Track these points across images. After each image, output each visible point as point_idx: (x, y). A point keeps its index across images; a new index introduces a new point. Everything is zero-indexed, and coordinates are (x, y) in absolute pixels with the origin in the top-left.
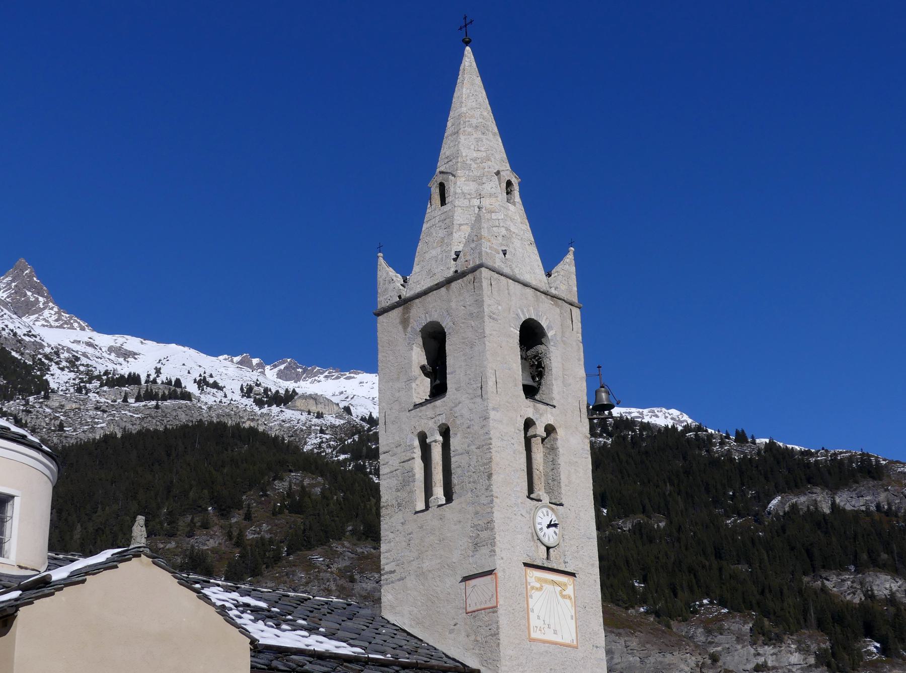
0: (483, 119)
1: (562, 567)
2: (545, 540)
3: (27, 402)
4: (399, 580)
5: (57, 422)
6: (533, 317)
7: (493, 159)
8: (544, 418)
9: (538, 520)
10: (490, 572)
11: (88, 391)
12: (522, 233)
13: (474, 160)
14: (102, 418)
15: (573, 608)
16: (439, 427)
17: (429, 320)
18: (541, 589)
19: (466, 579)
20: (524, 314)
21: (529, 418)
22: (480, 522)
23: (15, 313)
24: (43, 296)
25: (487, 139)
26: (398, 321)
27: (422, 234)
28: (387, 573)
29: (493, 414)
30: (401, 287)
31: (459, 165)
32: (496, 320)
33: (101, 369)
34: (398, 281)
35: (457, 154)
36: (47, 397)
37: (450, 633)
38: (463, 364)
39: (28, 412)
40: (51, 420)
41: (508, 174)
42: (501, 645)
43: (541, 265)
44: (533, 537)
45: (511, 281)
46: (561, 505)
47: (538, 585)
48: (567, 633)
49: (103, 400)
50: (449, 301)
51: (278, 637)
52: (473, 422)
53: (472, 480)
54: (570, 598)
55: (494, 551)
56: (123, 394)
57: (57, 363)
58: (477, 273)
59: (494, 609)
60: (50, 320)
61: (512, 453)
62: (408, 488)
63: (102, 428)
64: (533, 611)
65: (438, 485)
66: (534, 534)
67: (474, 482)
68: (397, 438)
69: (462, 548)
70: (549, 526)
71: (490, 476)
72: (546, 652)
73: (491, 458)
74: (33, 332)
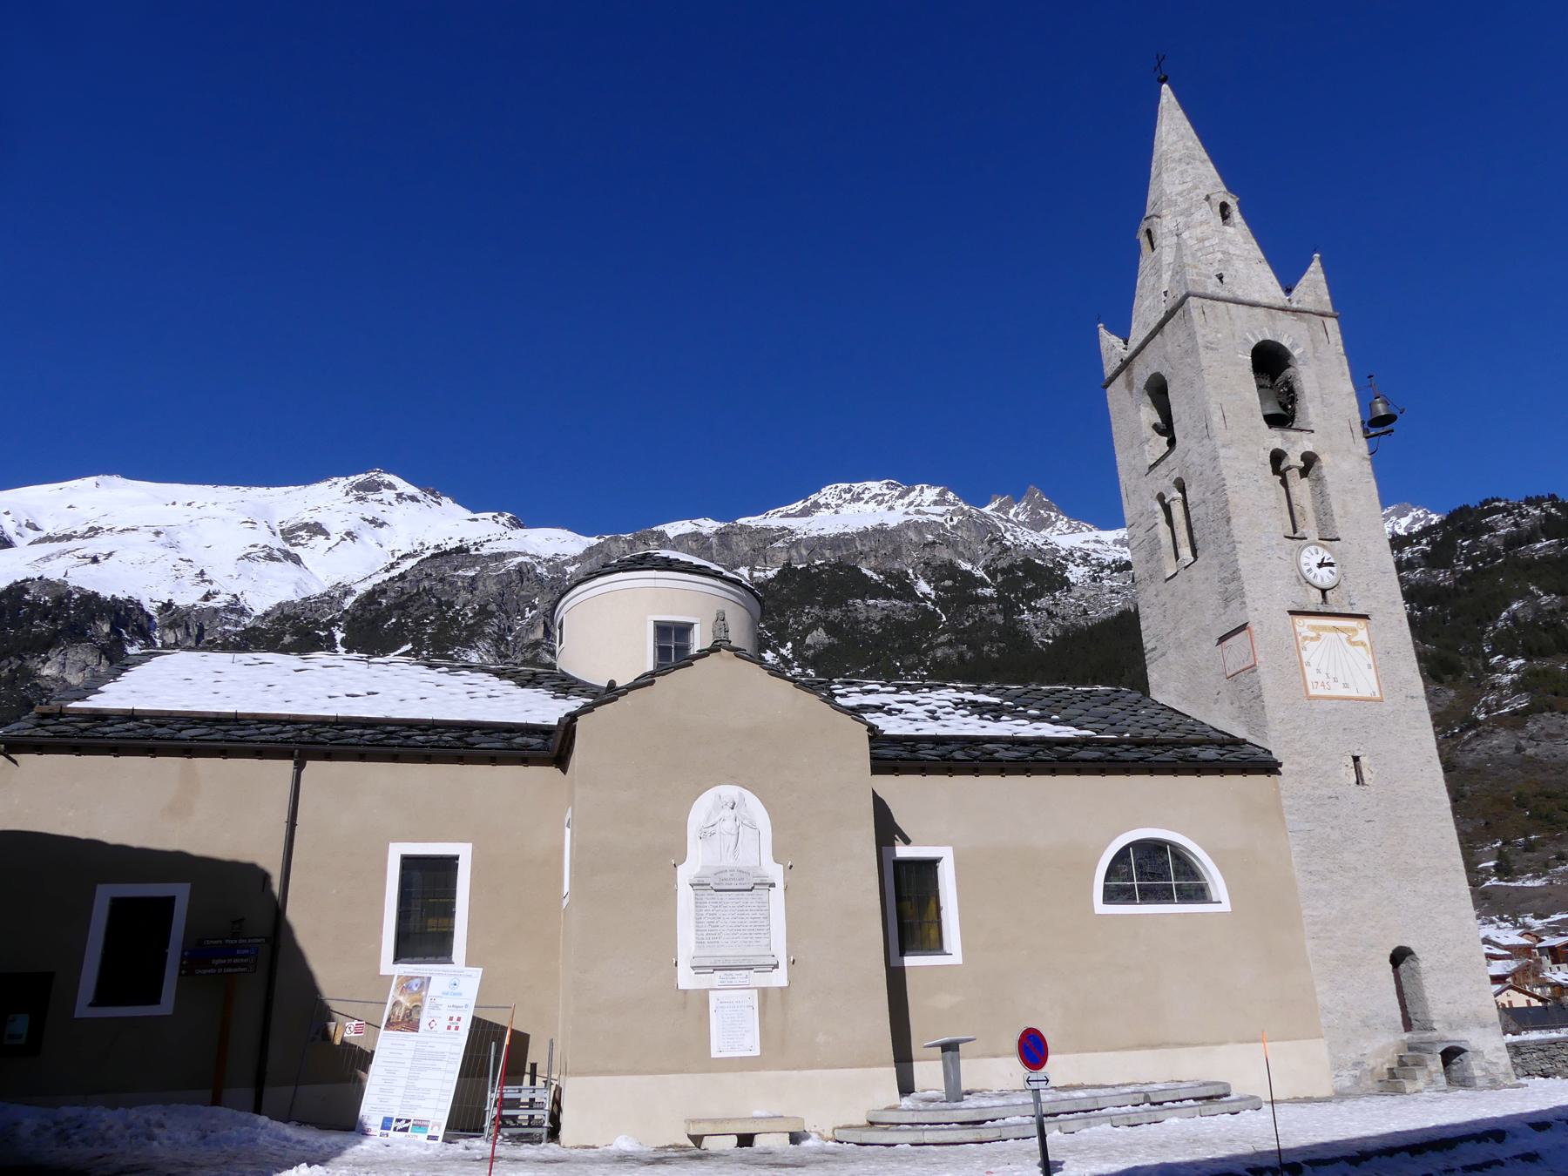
0: (1187, 149)
1: (1348, 610)
2: (1318, 582)
3: (1055, 597)
4: (1161, 656)
5: (1082, 609)
6: (1269, 337)
7: (1201, 187)
8: (1295, 446)
9: (1303, 560)
10: (1243, 627)
11: (1102, 579)
12: (1246, 253)
13: (1180, 194)
14: (1118, 599)
15: (1370, 656)
16: (1174, 483)
17: (1150, 373)
18: (1318, 637)
19: (1222, 639)
20: (1254, 335)
21: (1277, 449)
22: (1226, 574)
23: (1033, 529)
24: (1054, 511)
25: (1193, 168)
26: (1124, 385)
27: (1137, 289)
28: (1149, 651)
29: (1222, 452)
30: (1123, 351)
31: (1164, 204)
32: (1216, 349)
33: (1110, 559)
34: (1120, 346)
35: (1162, 193)
36: (1069, 590)
37: (1215, 704)
38: (1187, 407)
39: (1057, 605)
40: (1076, 607)
41: (1221, 194)
42: (1266, 708)
43: (1276, 281)
44: (1299, 580)
45: (1232, 304)
46: (1338, 539)
47: (1313, 634)
48: (1365, 683)
49: (1115, 584)
50: (1165, 346)
51: (985, 727)
52: (1204, 468)
53: (1212, 530)
54: (1363, 644)
55: (1244, 603)
56: (1131, 576)
57: (1073, 562)
58: (1185, 305)
59: (1253, 668)
60: (1062, 529)
61: (1257, 490)
62: (1155, 557)
63: (1119, 606)
64: (1308, 664)
65: (1182, 545)
66: (1300, 577)
67: (1214, 532)
68: (1139, 508)
69: (1213, 607)
70: (1320, 565)
71: (1228, 520)
72: (1336, 710)
73: (1227, 500)
74: (1049, 541)
